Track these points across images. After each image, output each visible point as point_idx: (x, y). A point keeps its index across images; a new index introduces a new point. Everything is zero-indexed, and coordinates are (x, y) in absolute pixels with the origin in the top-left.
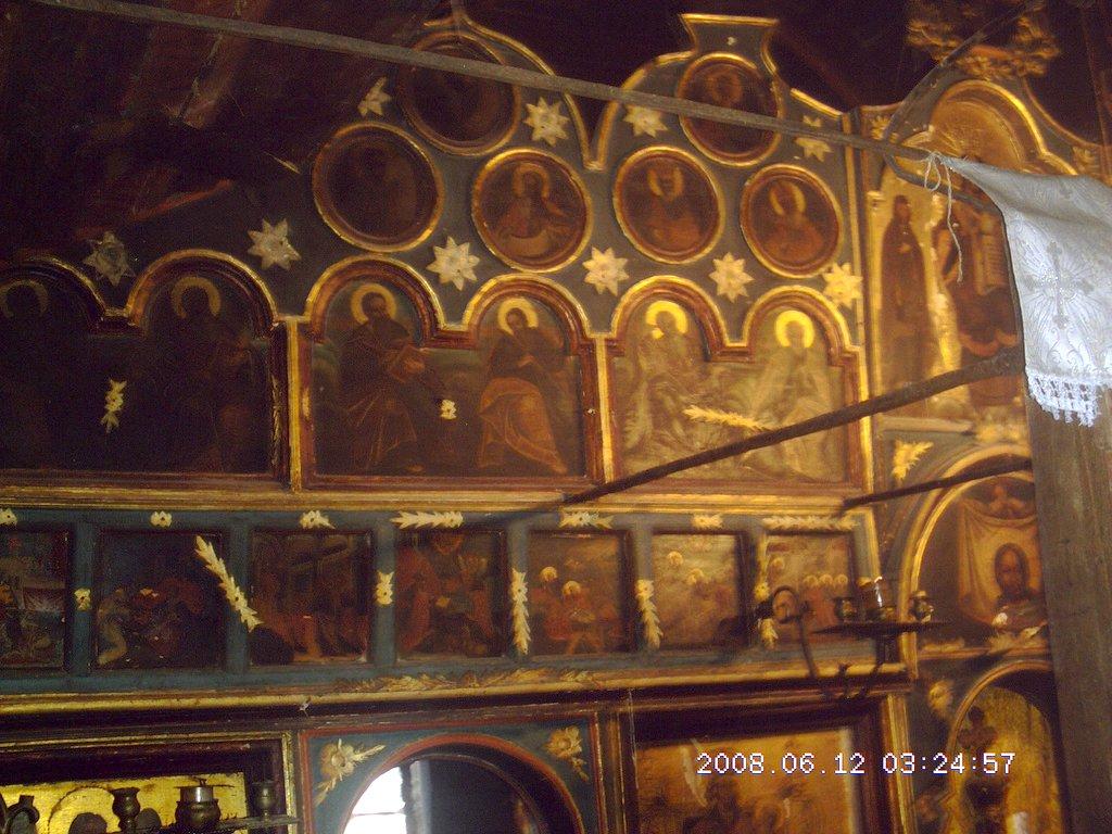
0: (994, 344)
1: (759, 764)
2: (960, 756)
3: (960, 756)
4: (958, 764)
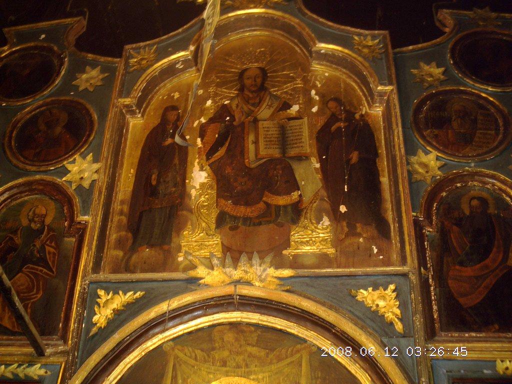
1: (350, 352)
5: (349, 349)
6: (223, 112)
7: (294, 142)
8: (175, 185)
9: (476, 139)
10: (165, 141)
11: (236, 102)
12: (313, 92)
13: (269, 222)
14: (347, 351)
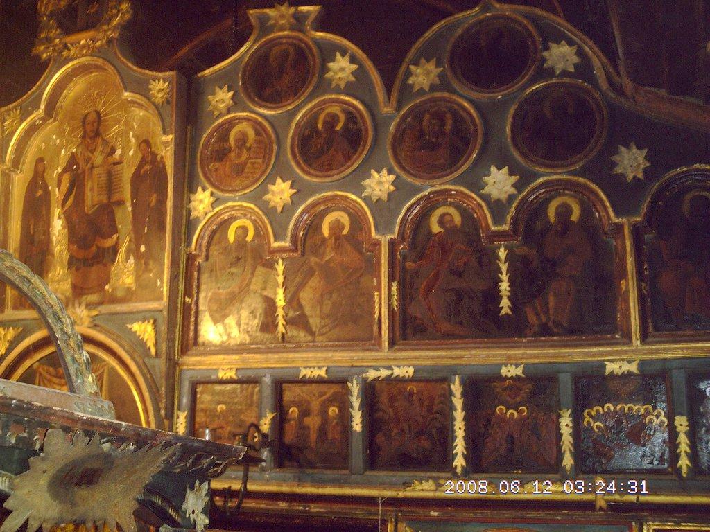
0: (94, 249)
1: (485, 487)
2: (613, 482)
3: (613, 482)
4: (612, 487)
5: (484, 484)
6: (73, 159)
7: (116, 187)
8: (44, 235)
9: (246, 170)
10: (36, 193)
11: (80, 150)
12: (131, 134)
13: (98, 263)
14: (482, 487)
